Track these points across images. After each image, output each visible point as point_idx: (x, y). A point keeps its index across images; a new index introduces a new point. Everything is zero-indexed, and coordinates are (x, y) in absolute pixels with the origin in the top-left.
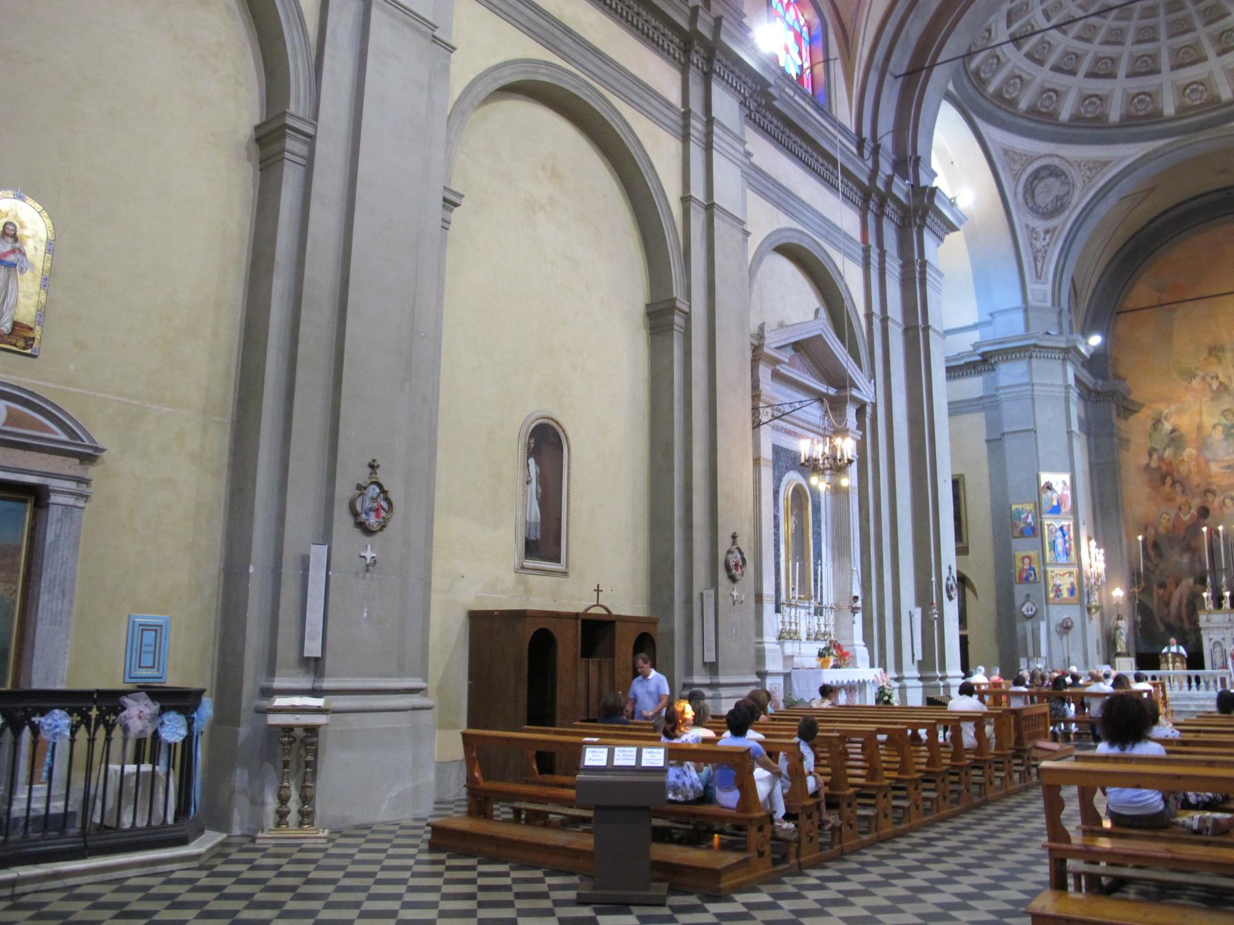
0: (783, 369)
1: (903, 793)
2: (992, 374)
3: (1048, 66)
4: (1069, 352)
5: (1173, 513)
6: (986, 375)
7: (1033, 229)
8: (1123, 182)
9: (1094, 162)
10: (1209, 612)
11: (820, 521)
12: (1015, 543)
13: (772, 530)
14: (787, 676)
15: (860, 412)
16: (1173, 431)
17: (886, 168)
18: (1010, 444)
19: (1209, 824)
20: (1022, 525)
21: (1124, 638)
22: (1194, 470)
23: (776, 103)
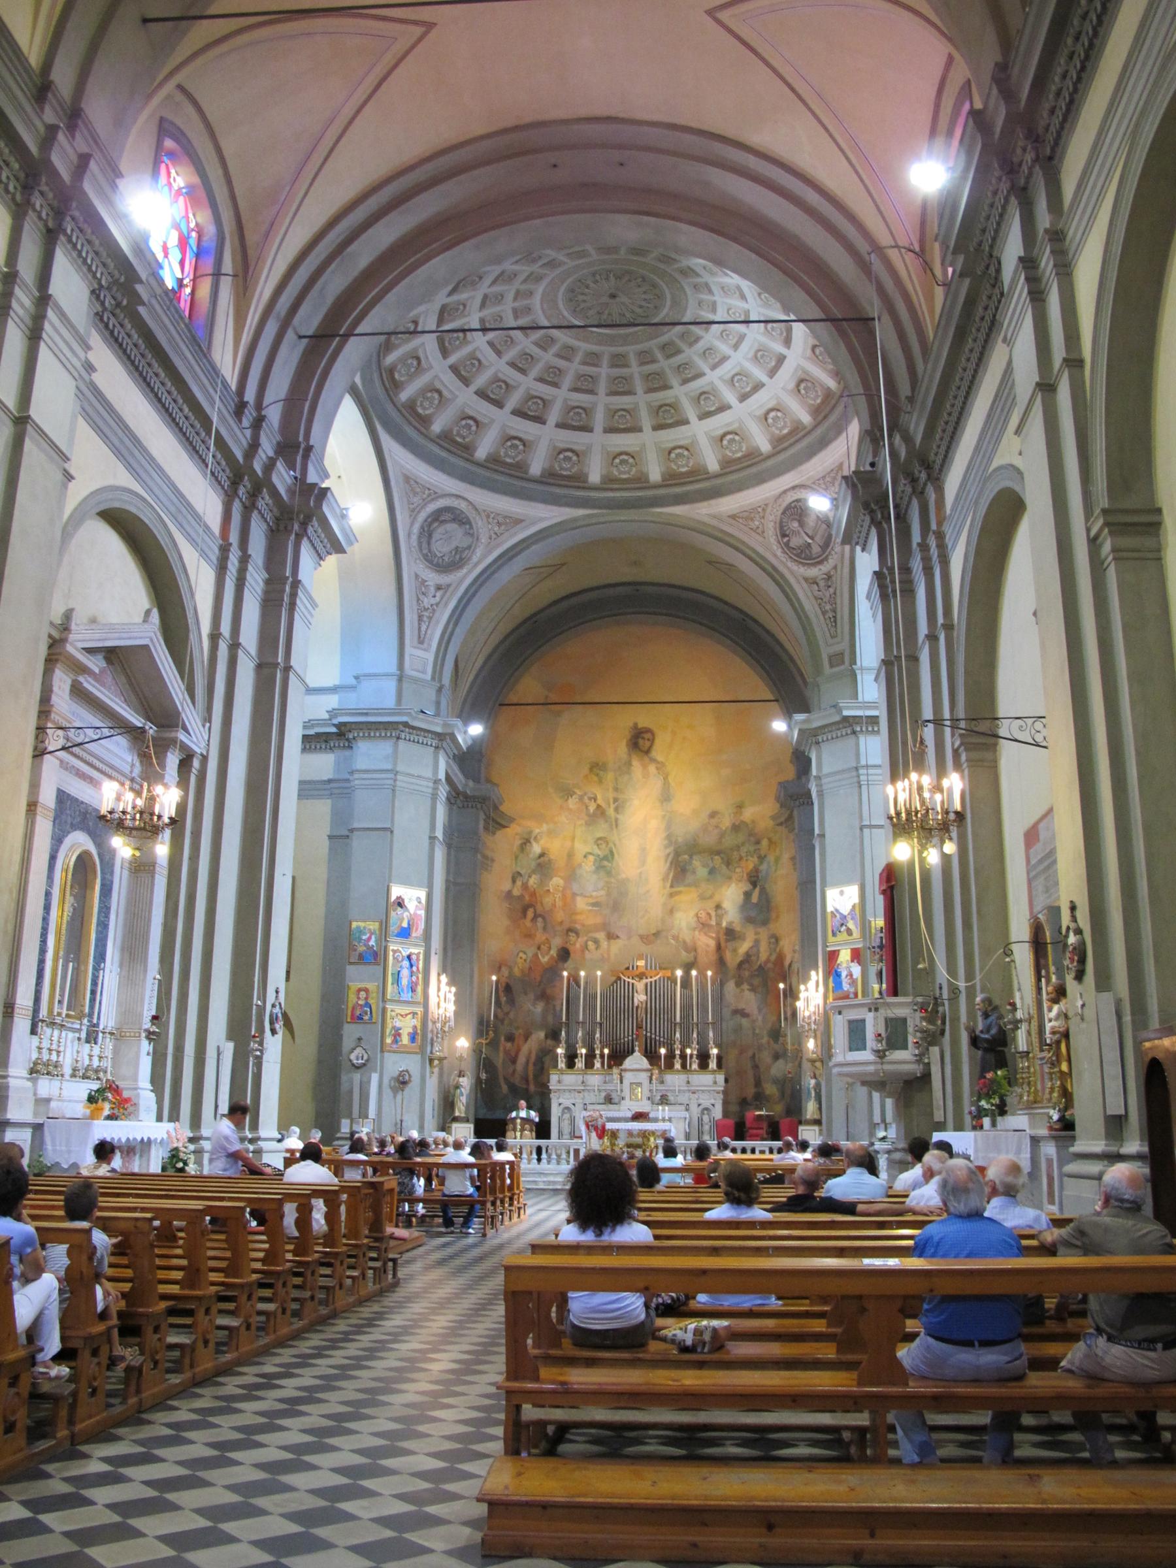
0: (88, 684)
1: (231, 1306)
2: (347, 753)
3: (473, 388)
4: (443, 739)
5: (531, 952)
6: (339, 752)
7: (424, 581)
8: (534, 547)
9: (506, 517)
10: (562, 1072)
11: (108, 909)
12: (351, 970)
13: (41, 912)
14: (38, 1128)
15: (185, 764)
16: (542, 855)
17: (267, 448)
18: (358, 844)
19: (707, 1337)
20: (362, 949)
21: (464, 1099)
22: (559, 903)
23: (142, 310)
